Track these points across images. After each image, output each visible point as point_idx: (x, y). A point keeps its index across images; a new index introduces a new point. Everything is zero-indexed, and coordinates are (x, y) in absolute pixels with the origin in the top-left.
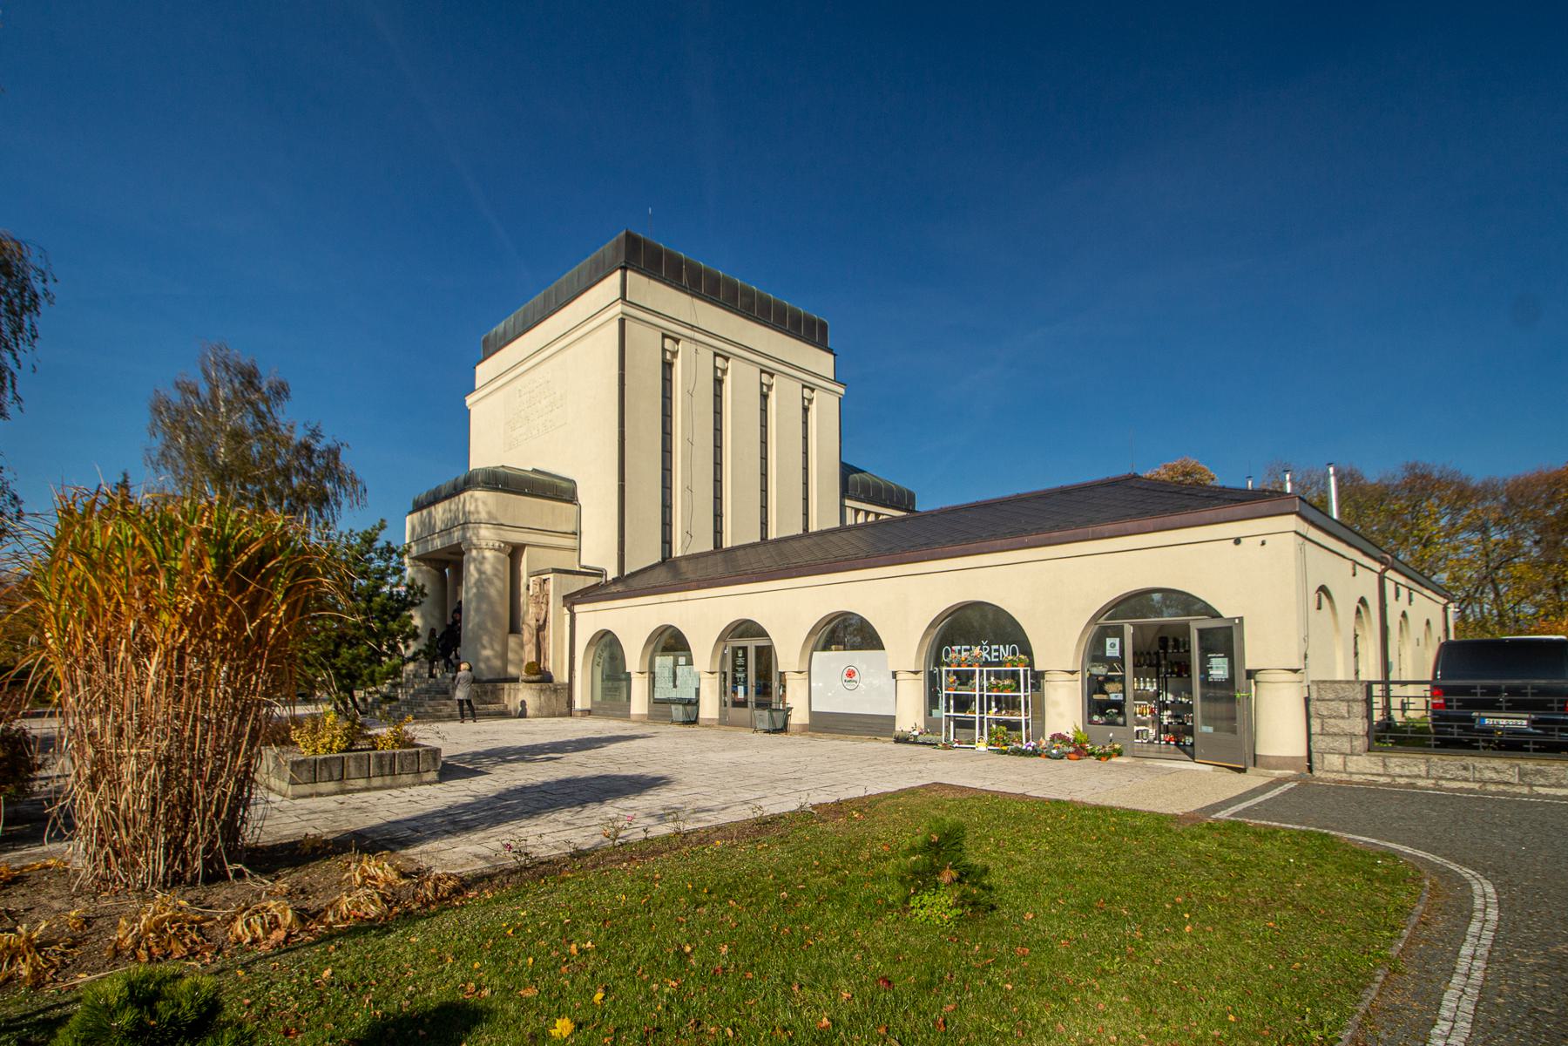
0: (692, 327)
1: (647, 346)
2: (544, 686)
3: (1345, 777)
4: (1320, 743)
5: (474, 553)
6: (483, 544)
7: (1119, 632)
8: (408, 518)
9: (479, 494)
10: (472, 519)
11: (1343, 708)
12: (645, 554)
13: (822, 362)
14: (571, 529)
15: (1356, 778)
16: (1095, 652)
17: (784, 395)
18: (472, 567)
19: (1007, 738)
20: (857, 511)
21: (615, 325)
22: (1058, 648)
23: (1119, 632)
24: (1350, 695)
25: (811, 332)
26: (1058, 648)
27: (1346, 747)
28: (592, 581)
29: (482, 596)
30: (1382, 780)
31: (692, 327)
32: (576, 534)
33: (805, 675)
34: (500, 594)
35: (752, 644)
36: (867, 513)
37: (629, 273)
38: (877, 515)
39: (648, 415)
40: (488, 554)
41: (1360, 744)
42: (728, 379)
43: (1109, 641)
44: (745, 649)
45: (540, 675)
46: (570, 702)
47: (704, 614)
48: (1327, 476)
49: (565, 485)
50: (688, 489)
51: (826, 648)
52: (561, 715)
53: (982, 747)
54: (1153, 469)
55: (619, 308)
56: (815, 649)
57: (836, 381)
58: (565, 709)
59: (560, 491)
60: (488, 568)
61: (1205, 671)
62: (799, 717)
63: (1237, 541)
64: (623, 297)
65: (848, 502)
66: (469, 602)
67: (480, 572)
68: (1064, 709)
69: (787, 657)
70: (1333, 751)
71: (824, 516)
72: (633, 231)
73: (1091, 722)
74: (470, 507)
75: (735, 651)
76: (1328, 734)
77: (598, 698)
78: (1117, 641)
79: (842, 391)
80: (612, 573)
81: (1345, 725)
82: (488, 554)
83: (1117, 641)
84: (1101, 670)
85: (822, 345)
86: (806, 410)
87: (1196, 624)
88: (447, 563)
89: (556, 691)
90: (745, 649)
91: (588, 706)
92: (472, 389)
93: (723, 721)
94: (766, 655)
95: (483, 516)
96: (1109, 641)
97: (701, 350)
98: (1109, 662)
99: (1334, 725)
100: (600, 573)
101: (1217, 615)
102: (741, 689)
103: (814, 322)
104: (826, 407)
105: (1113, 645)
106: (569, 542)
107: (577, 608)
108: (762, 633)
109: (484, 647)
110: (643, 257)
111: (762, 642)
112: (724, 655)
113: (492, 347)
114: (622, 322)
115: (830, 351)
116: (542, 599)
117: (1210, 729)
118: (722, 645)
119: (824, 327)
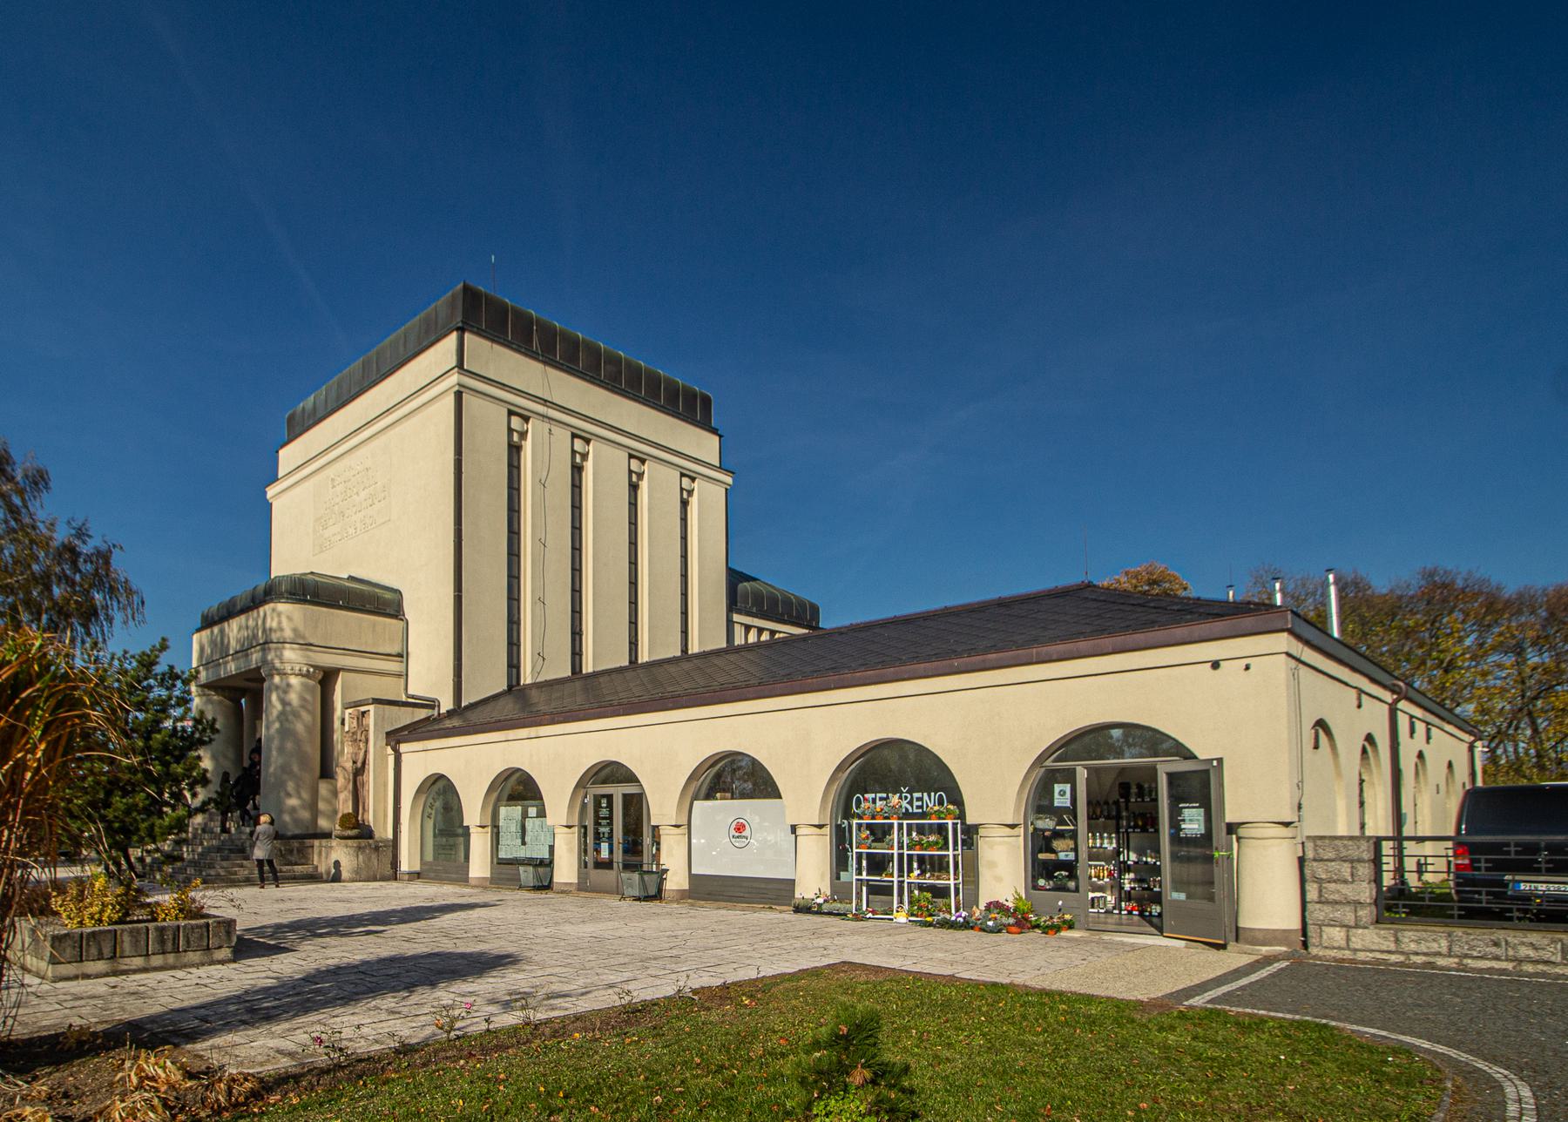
0: (545, 402)
1: (488, 421)
2: (363, 842)
3: (1348, 954)
4: (1317, 913)
5: (277, 679)
6: (288, 669)
7: (1069, 776)
8: (196, 637)
9: (283, 607)
10: (274, 637)
11: (1346, 870)
12: (487, 680)
13: (706, 446)
14: (396, 649)
15: (1361, 956)
16: (1040, 801)
17: (658, 485)
18: (274, 697)
19: (933, 908)
20: (748, 628)
21: (450, 400)
22: (994, 796)
23: (1069, 776)
24: (1355, 854)
25: (690, 407)
26: (994, 796)
27: (1350, 918)
28: (422, 714)
29: (286, 733)
30: (1393, 958)
31: (545, 402)
32: (402, 656)
33: (684, 830)
34: (309, 729)
35: (618, 791)
36: (761, 631)
37: (467, 335)
38: (773, 633)
39: (489, 509)
40: (294, 681)
41: (1366, 914)
42: (589, 466)
43: (1057, 788)
44: (610, 798)
45: (357, 829)
46: (395, 863)
47: (559, 755)
48: (1325, 585)
49: (388, 595)
50: (540, 601)
51: (709, 796)
52: (383, 879)
53: (901, 918)
54: (1110, 576)
55: (454, 378)
56: (695, 798)
57: (721, 468)
58: (388, 871)
59: (382, 603)
60: (293, 697)
61: (1175, 825)
62: (676, 881)
63: (1216, 665)
64: (460, 365)
65: (736, 617)
66: (270, 739)
67: (284, 703)
68: (1003, 872)
69: (662, 807)
70: (1333, 923)
71: (706, 634)
72: (472, 283)
73: (1035, 887)
74: (272, 623)
75: (597, 799)
76: (1327, 902)
77: (429, 857)
78: (1067, 787)
79: (729, 480)
80: (447, 704)
81: (1347, 891)
82: (294, 681)
83: (1067, 787)
84: (1047, 824)
85: (705, 424)
86: (685, 504)
87: (1165, 767)
88: (243, 692)
89: (377, 848)
90: (610, 798)
91: (417, 868)
92: (274, 479)
93: (583, 886)
94: (635, 805)
95: (288, 634)
96: (1057, 788)
97: (556, 430)
98: (1057, 813)
99: (1334, 891)
100: (432, 704)
101: (1190, 756)
102: (605, 846)
103: (695, 395)
104: (709, 501)
105: (1062, 793)
106: (393, 666)
107: (403, 747)
108: (631, 778)
109: (289, 795)
110: (483, 316)
111: (631, 789)
112: (584, 806)
113: (298, 427)
114: (459, 396)
115: (714, 431)
116: (359, 736)
117: (1182, 896)
118: (582, 792)
119: (706, 401)
